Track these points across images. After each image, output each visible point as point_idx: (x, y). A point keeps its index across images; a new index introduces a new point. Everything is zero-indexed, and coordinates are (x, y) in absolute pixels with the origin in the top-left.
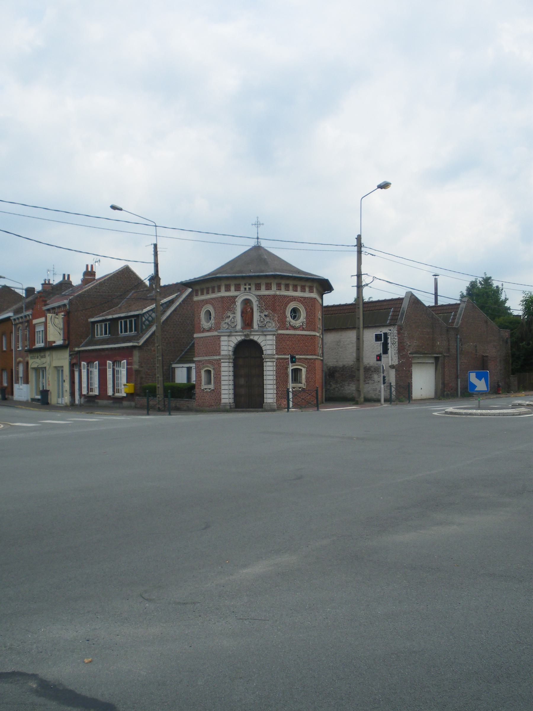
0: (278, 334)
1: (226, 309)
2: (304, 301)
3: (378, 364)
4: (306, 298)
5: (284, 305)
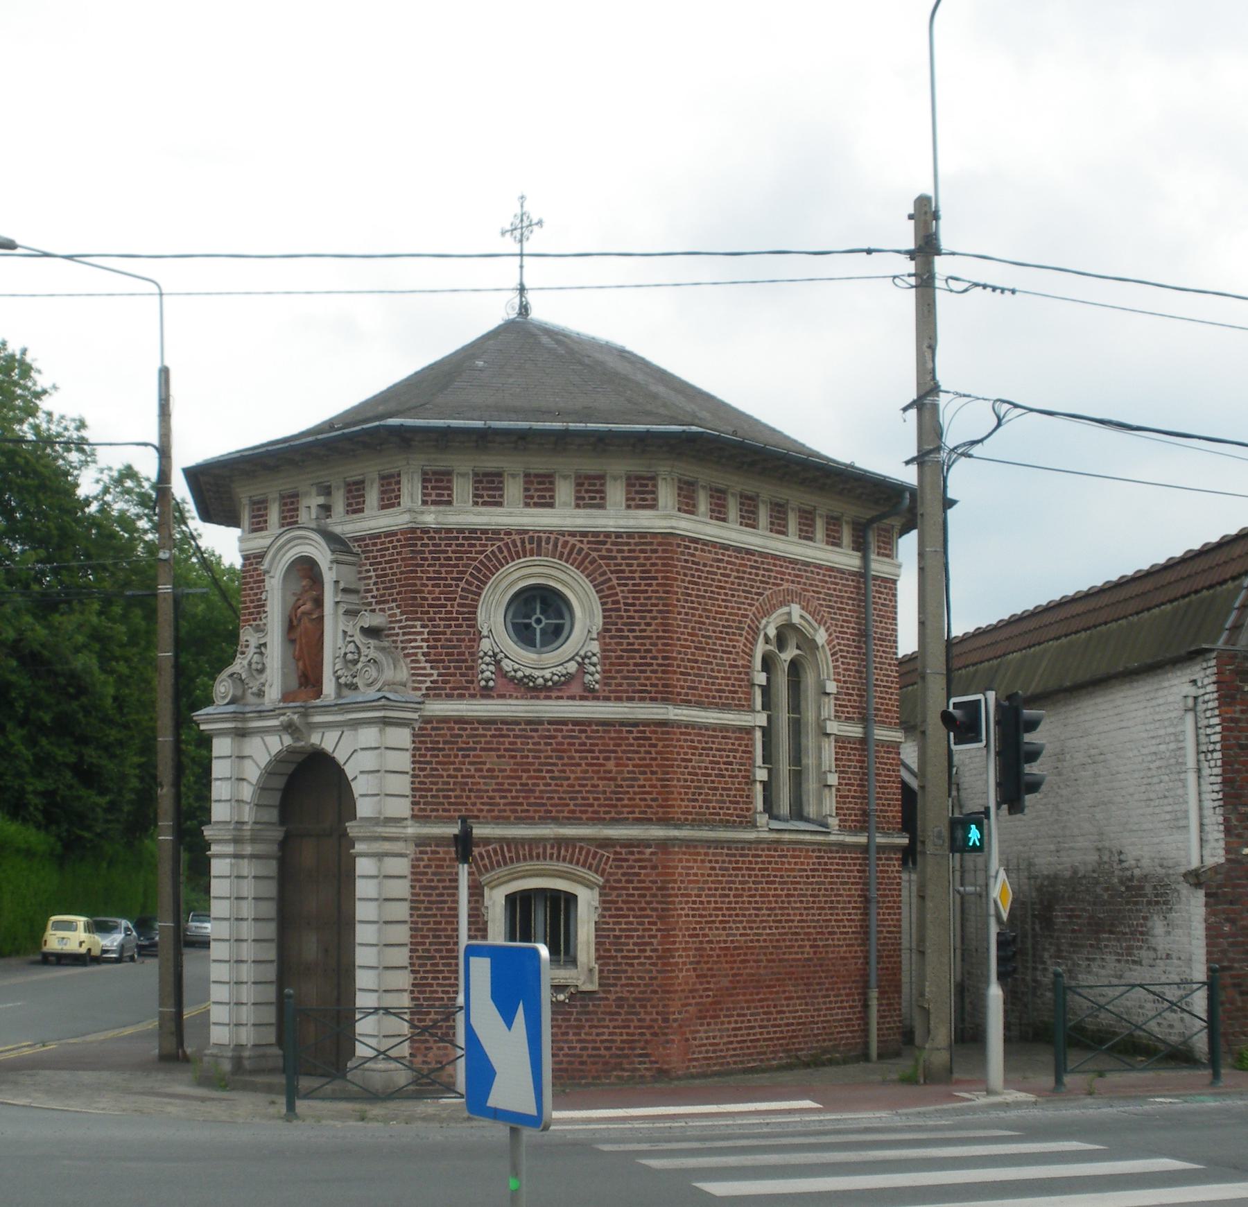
0: (427, 720)
2: (594, 554)
4: (608, 535)
5: (467, 576)
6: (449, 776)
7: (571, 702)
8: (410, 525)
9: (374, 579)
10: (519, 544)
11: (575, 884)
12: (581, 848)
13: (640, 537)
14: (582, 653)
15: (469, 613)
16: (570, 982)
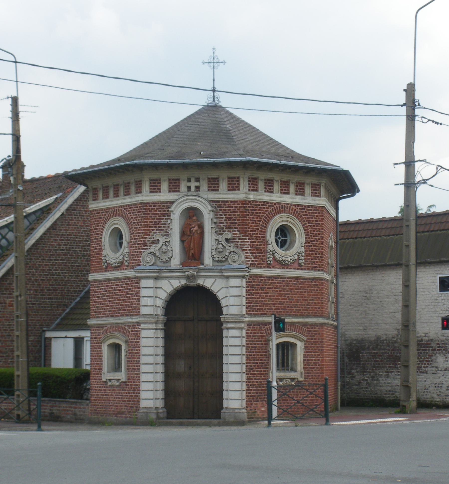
0: (251, 276)
1: (152, 227)
2: (301, 213)
3: (445, 335)
4: (305, 206)
5: (262, 220)
6: (259, 298)
7: (295, 271)
8: (245, 199)
9: (224, 219)
10: (278, 208)
11: (297, 340)
12: (298, 326)
13: (315, 208)
14: (299, 252)
15: (263, 234)
16: (296, 377)
